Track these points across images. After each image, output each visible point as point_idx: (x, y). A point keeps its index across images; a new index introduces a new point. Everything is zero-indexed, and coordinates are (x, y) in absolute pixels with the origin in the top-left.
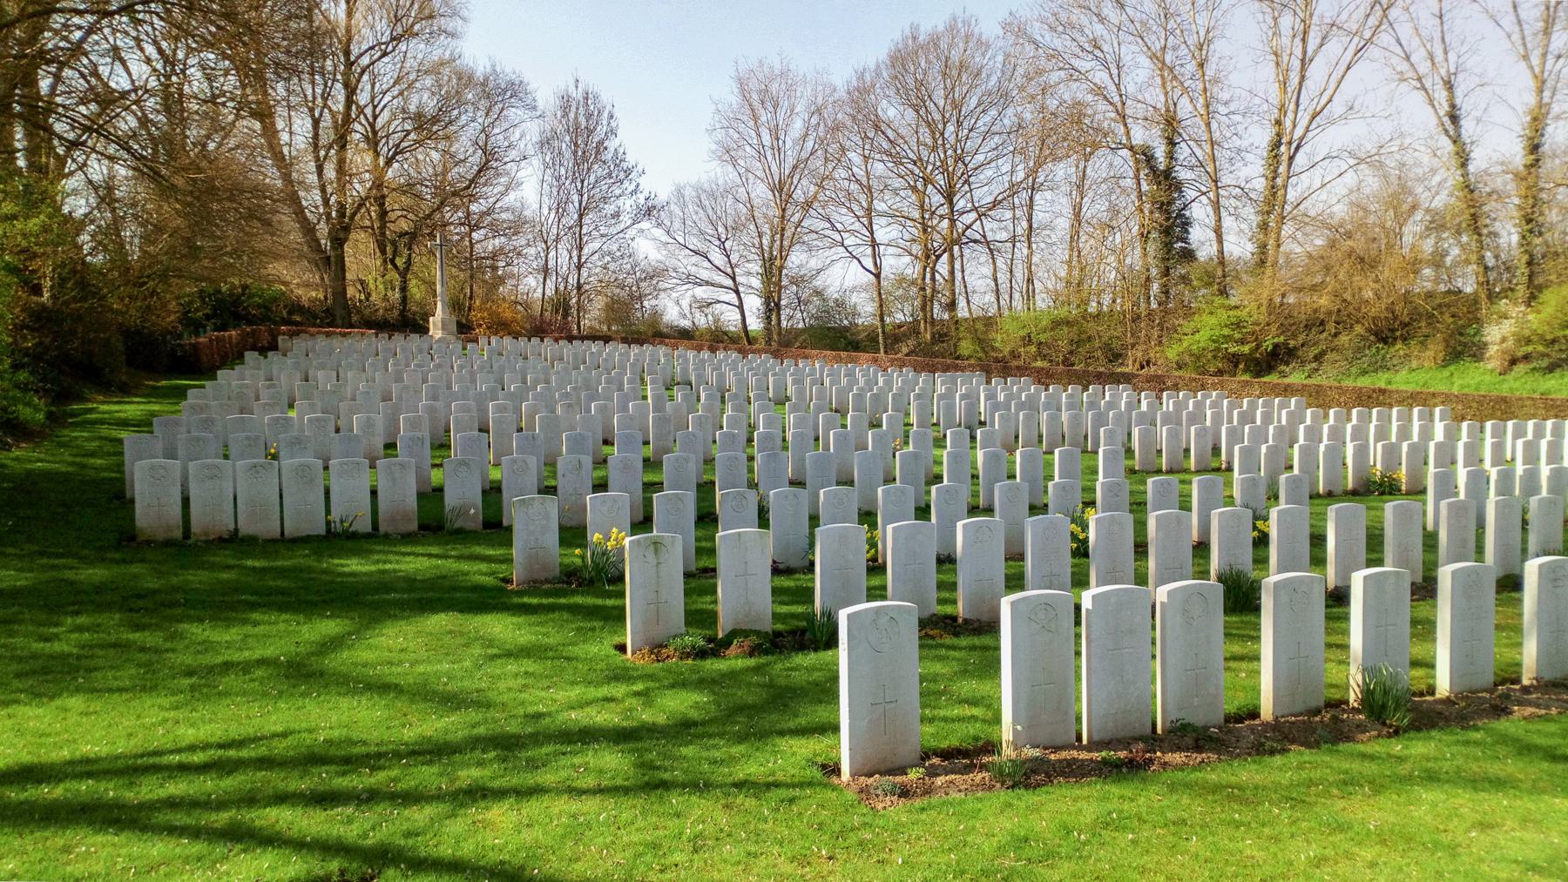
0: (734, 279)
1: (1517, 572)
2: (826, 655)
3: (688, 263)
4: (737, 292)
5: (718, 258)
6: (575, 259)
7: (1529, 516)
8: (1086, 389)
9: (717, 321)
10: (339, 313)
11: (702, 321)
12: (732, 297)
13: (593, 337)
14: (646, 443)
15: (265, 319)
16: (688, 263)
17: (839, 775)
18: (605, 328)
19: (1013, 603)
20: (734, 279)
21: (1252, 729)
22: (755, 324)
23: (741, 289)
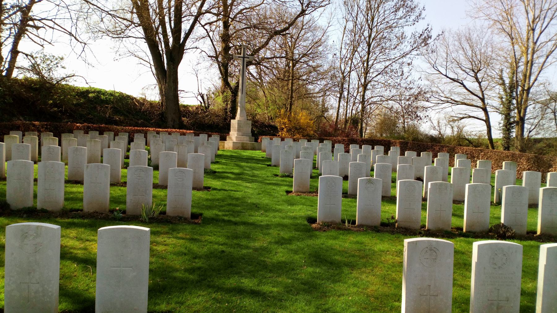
0: (483, 100)
2: (315, 198)
3: (447, 88)
4: (485, 110)
5: (473, 85)
6: (363, 81)
7: (332, 154)
8: (435, 156)
11: (448, 132)
12: (482, 115)
14: (390, 199)
16: (447, 88)
17: (223, 139)
18: (379, 135)
20: (483, 100)
21: (424, 230)
22: (497, 134)
23: (489, 109)
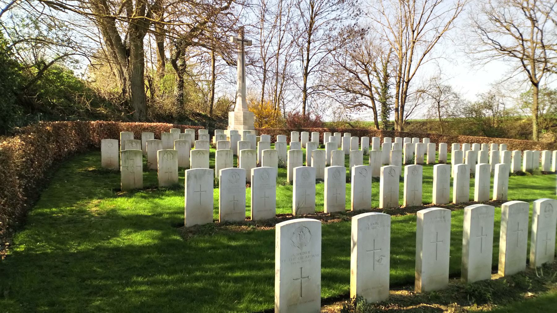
10: (137, 106)
12: (370, 103)
15: (68, 111)
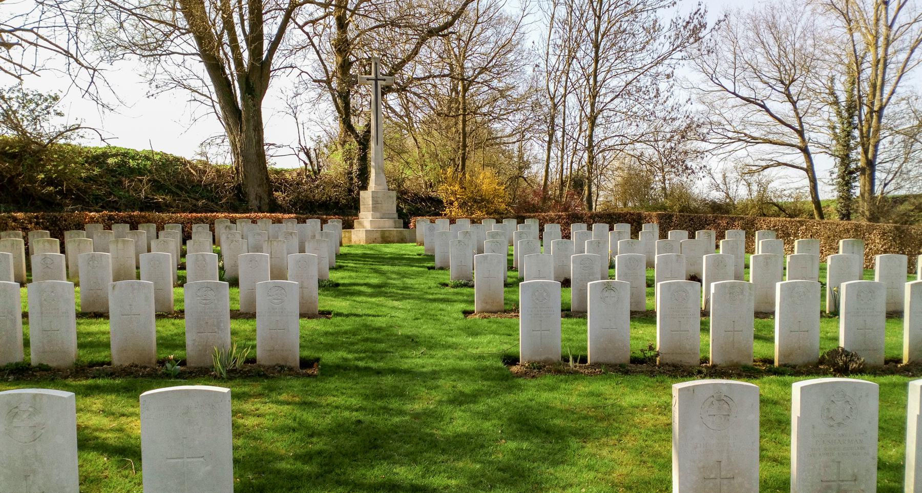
0: (801, 133)
1: (899, 309)
3: (734, 113)
4: (805, 150)
9: (763, 187)
11: (741, 193)
13: (610, 218)
19: (802, 388)
20: (801, 133)
22: (828, 193)
23: (811, 149)
